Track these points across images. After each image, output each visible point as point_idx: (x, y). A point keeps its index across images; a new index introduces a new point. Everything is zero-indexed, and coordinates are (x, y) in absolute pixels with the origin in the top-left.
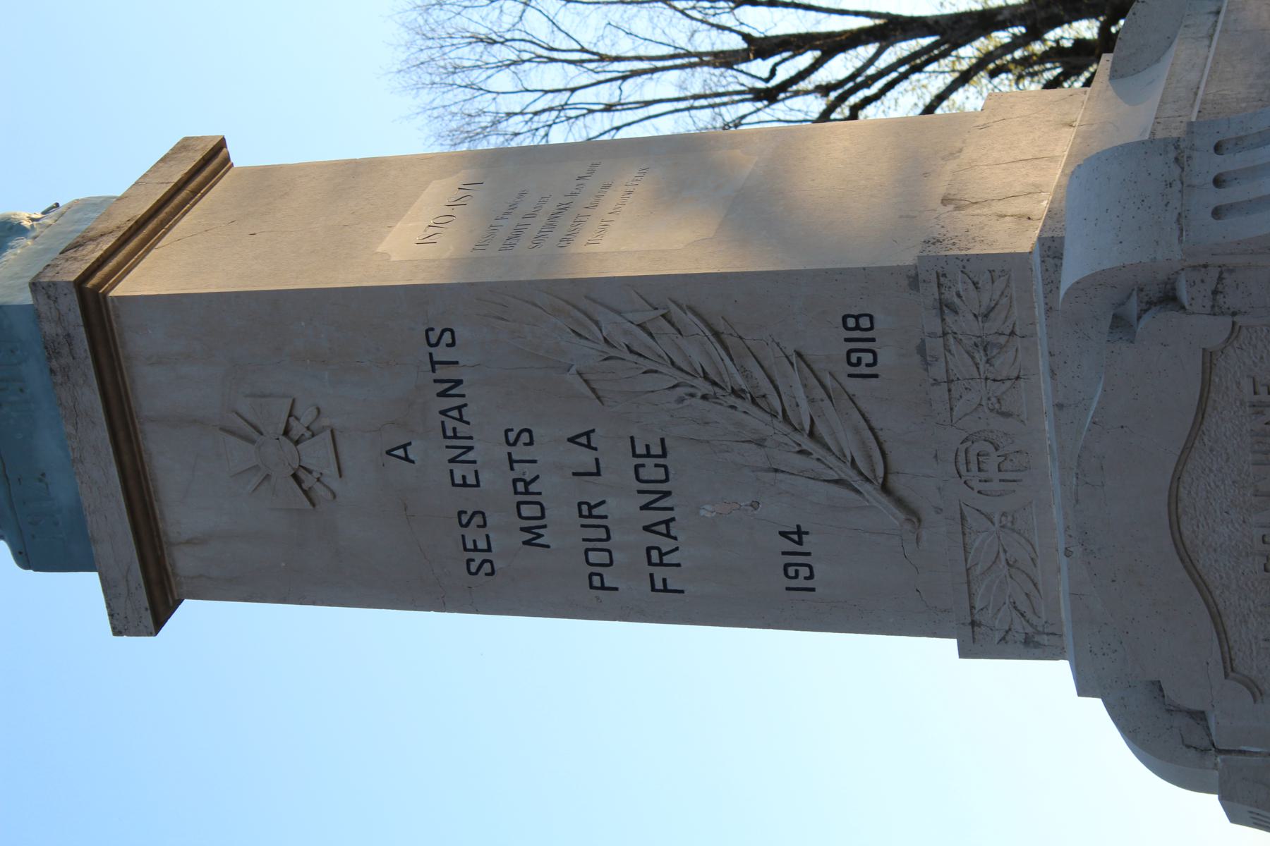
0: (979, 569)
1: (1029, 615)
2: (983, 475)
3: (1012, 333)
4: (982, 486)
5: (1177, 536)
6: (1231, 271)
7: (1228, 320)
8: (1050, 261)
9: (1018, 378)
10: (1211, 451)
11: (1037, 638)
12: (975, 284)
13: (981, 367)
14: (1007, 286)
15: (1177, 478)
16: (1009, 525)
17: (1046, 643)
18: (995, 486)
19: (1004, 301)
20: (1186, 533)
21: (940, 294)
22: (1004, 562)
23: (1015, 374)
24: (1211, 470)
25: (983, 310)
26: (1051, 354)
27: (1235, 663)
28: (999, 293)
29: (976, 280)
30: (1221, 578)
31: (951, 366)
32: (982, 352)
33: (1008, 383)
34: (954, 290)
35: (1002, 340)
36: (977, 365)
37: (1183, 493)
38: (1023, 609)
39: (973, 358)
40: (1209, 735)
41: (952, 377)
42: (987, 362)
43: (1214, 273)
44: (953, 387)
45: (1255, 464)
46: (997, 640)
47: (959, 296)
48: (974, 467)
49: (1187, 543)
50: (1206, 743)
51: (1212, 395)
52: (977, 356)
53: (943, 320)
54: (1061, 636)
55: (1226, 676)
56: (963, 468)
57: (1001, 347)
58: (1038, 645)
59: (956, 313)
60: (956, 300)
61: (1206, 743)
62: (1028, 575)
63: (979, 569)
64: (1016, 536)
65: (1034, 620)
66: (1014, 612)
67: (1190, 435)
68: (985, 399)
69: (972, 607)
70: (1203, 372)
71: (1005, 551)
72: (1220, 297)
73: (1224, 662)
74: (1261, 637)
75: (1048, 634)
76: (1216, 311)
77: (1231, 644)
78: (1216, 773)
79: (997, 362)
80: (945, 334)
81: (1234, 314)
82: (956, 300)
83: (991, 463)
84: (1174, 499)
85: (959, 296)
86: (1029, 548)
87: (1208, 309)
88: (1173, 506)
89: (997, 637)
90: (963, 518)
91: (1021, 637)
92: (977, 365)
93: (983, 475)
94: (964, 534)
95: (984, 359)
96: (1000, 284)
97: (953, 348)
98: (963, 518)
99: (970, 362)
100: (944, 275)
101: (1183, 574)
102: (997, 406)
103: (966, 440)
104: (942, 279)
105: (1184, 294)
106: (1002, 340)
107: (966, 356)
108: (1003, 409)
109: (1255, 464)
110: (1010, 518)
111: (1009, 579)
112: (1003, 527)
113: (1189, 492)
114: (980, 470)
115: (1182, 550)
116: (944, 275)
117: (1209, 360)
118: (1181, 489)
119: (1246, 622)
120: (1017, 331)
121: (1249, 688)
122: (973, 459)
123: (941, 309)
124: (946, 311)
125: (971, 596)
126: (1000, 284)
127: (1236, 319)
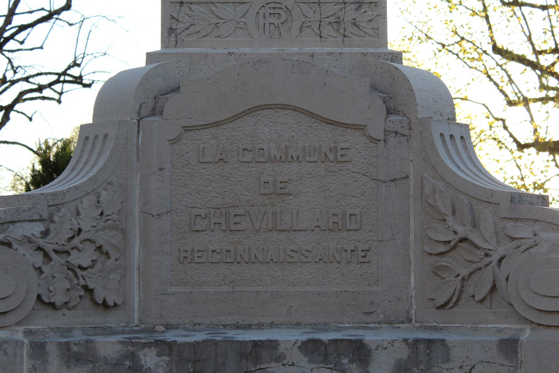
0: (213, 8)
1: (187, 32)
2: (267, 15)
3: (345, 36)
4: (261, 15)
5: (264, 107)
6: (407, 140)
7: (382, 137)
8: (390, 57)
9: (321, 37)
10: (310, 126)
11: (173, 35)
12: (371, 20)
13: (326, 19)
14: (370, 35)
15: (295, 109)
16: (239, 26)
17: (171, 39)
18: (262, 21)
19: (362, 33)
20: (265, 112)
21: (366, 3)
22: (218, 21)
23: (323, 35)
24: (299, 126)
25: (357, 23)
26: (341, 54)
27: (190, 132)
28: (367, 31)
29: (373, 21)
30: (239, 128)
31: (328, 5)
32: (335, 21)
33: (318, 32)
34: (368, 10)
35: (342, 31)
36: (328, 17)
37: (287, 112)
38: (191, 29)
39: (332, 16)
40: (146, 117)
41: (321, 5)
42: (330, 23)
43: (407, 132)
44: (316, 5)
45: (304, 148)
46: (172, 14)
47: (365, 12)
48: (272, 11)
49: (258, 112)
50: (142, 115)
51: (340, 129)
52: (333, 18)
53: (352, 3)
54: (175, 47)
55: (183, 127)
56: (271, 5)
57: (338, 31)
58: (169, 35)
59: (356, 10)
60: (363, 10)
61: (142, 115)
62: (210, 33)
63: (213, 8)
64: (233, 29)
65: (184, 34)
66: (189, 24)
67: (320, 116)
68: (310, 20)
69: (191, 3)
70: (354, 125)
71: (224, 23)
72: (394, 134)
73: (191, 127)
74: (205, 145)
75: (176, 41)
76: (387, 132)
77: (201, 131)
78: (129, 119)
79: (329, 27)
80: (345, 3)
81: (385, 141)
82: (363, 10)
83: (273, 20)
84: (284, 107)
85: (365, 12)
86: (226, 35)
87: (387, 129)
88: (280, 106)
89: (175, 15)
90: (243, 3)
91: (174, 26)
92: (328, 17)
93: (267, 15)
94: (234, 3)
95: (332, 21)
96: (371, 32)
97: (337, 7)
98: (243, 3)
99: (331, 14)
100: (376, 6)
101: (242, 109)
102: (306, 25)
103: (287, 9)
104: (374, 5)
105: (393, 118)
106: (342, 31)
107: (333, 13)
108: (304, 29)
109: (304, 148)
110: (243, 26)
111: (208, 23)
112: (238, 23)
113: (287, 115)
114: (270, 14)
115: (255, 109)
116: (376, 6)
117: (360, 128)
118: (289, 111)
119: (214, 138)
120: (346, 39)
121: (176, 138)
122: (277, 11)
123: (359, 3)
124: (357, 5)
125: (198, 3)
126: (371, 32)
127: (382, 142)
